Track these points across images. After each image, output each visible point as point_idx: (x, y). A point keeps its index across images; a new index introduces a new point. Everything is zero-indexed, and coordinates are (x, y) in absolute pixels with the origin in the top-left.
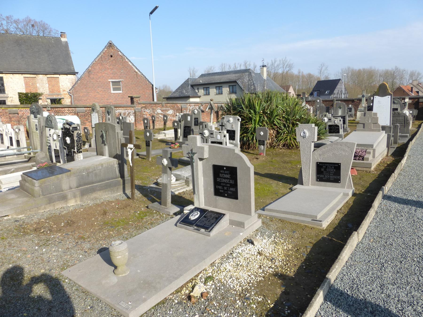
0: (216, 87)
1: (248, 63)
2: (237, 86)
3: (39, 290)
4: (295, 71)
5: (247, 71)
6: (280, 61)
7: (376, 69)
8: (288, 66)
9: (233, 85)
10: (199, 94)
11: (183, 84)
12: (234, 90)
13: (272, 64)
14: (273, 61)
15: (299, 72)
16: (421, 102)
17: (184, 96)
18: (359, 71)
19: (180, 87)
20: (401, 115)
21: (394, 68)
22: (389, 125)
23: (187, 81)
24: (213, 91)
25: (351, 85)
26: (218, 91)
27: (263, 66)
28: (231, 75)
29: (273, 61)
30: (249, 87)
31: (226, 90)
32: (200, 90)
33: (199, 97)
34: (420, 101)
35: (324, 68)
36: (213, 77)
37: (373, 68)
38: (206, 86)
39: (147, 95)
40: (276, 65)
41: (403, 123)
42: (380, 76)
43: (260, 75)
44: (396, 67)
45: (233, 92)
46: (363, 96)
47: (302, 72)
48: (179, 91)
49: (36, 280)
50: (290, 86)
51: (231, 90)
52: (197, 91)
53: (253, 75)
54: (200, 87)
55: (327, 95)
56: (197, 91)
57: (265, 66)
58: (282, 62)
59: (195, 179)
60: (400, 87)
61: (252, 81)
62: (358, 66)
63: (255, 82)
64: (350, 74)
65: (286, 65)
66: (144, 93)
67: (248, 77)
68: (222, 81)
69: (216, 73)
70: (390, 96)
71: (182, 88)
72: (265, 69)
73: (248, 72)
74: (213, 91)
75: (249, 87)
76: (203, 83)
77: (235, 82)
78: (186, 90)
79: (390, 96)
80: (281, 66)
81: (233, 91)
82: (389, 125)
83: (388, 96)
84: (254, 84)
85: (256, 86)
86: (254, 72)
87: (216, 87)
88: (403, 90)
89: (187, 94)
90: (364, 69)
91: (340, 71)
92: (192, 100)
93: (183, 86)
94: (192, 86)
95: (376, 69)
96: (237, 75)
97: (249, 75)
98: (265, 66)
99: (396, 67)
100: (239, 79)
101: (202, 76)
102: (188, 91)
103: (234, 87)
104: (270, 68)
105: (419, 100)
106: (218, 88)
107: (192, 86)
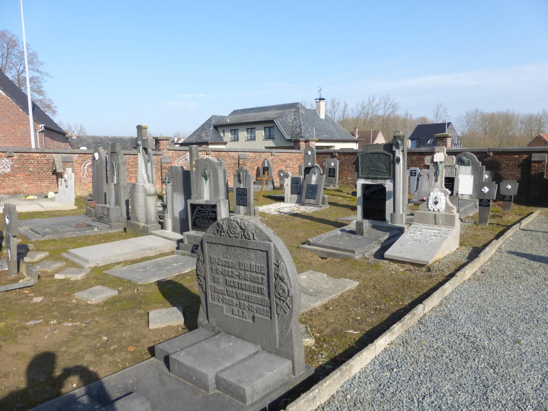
0: (247, 129)
1: (336, 101)
3: (73, 386)
4: (401, 113)
5: (294, 106)
6: (380, 99)
8: (391, 106)
9: (269, 125)
10: (225, 139)
11: (204, 125)
12: (272, 134)
13: (370, 103)
14: (371, 100)
15: (407, 115)
16: (535, 162)
17: (202, 141)
19: (199, 128)
21: (541, 112)
23: (210, 120)
24: (243, 135)
25: (480, 133)
26: (249, 135)
27: (320, 99)
28: (271, 112)
29: (371, 100)
30: (292, 130)
31: (260, 133)
32: (225, 133)
33: (225, 144)
34: (533, 159)
35: (441, 110)
36: (248, 114)
37: (511, 112)
38: (234, 127)
39: (19, 135)
40: (374, 104)
41: (265, 288)
42: (522, 123)
43: (314, 113)
44: (544, 110)
45: (269, 137)
47: (411, 115)
48: (197, 134)
49: (68, 372)
50: (378, 132)
51: (268, 134)
52: (222, 135)
53: (302, 111)
54: (226, 129)
55: (429, 145)
56: (222, 135)
57: (323, 99)
58: (383, 101)
60: (540, 136)
61: (298, 121)
63: (302, 123)
64: (478, 118)
65: (389, 104)
66: (13, 131)
67: (294, 115)
68: (255, 120)
69: (253, 108)
71: (201, 130)
72: (322, 103)
74: (243, 135)
76: (231, 123)
77: (272, 121)
78: (205, 133)
80: (382, 105)
81: (270, 136)
84: (301, 125)
85: (303, 128)
86: (304, 108)
87: (247, 129)
88: (545, 140)
89: (205, 139)
90: (499, 113)
91: (464, 114)
92: (210, 147)
93: (203, 128)
94: (216, 127)
96: (279, 112)
97: (295, 112)
98: (323, 99)
99: (544, 110)
100: (279, 117)
101: (235, 112)
102: (209, 135)
103: (271, 129)
104: (367, 108)
105: (530, 157)
106: (250, 130)
107: (216, 127)
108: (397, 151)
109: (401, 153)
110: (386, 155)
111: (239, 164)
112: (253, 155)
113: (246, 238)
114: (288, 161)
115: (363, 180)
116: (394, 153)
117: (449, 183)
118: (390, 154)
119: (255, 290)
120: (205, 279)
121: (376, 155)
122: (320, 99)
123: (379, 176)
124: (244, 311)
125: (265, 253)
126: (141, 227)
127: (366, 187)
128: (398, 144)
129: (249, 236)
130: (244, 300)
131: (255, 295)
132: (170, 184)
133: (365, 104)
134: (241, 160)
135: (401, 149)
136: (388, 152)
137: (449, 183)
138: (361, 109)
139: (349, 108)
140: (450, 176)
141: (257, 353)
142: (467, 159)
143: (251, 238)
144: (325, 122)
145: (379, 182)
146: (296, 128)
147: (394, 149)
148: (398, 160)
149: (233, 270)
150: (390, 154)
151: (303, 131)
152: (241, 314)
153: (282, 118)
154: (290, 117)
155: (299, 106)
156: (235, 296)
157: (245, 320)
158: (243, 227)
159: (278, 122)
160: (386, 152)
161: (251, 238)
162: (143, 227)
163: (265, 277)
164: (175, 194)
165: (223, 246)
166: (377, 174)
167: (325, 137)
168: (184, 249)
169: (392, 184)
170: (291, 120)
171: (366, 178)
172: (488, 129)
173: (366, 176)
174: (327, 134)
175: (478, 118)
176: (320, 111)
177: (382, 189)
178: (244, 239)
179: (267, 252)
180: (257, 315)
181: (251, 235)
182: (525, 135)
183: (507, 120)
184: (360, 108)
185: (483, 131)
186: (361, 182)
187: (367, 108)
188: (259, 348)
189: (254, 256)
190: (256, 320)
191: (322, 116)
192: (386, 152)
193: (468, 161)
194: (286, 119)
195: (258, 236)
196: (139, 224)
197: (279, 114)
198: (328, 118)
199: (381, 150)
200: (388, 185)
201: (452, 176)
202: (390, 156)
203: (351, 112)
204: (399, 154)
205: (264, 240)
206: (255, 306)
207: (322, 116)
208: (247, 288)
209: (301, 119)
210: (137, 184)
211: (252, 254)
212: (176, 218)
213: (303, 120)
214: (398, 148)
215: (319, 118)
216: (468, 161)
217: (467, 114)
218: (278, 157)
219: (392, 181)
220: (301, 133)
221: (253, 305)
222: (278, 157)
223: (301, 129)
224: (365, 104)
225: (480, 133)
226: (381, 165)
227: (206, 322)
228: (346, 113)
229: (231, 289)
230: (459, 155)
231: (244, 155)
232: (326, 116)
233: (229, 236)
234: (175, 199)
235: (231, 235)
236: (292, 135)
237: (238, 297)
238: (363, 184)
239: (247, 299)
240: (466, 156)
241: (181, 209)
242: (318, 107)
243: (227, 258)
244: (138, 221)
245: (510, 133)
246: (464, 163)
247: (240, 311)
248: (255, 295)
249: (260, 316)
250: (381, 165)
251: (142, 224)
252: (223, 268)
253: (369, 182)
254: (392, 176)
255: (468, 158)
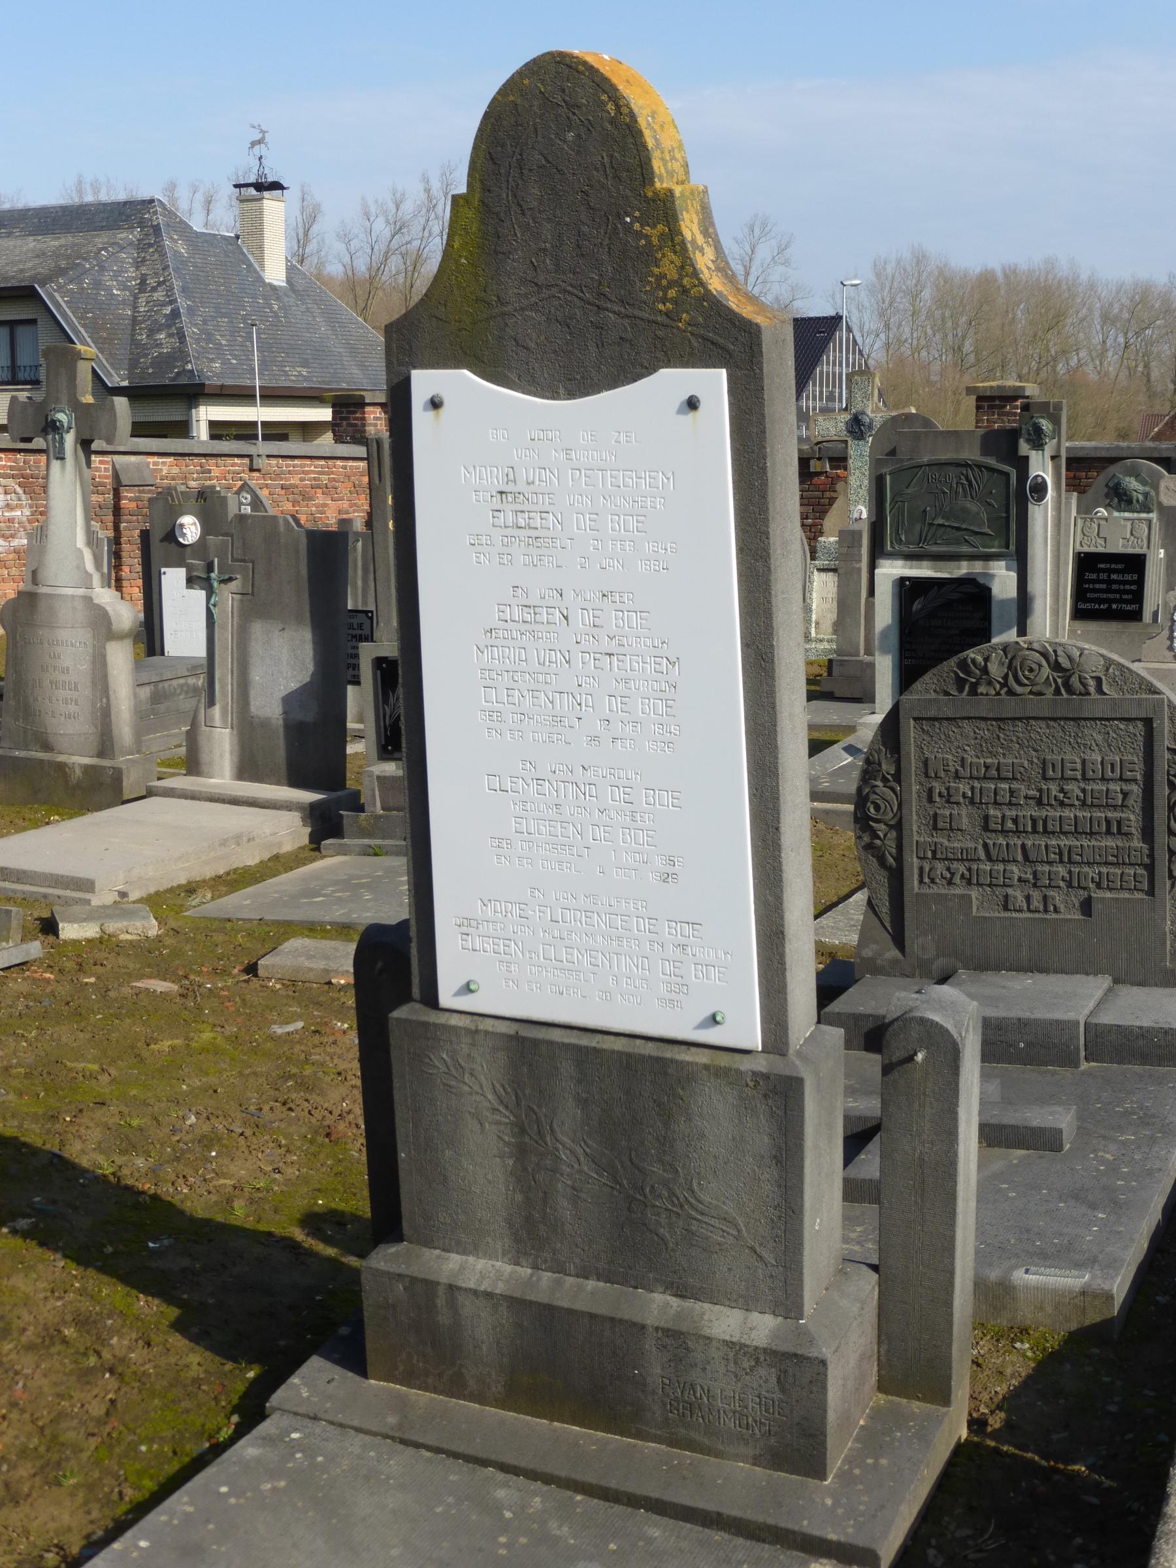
2: (43, 327)
5: (134, 215)
7: (1084, 277)
12: (23, 359)
18: (986, 281)
20: (1094, 706)
22: (746, 1029)
27: (260, 187)
30: (134, 342)
41: (1133, 818)
43: (235, 254)
46: (857, 427)
53: (174, 245)
57: (276, 186)
59: (1062, 562)
61: (159, 295)
62: (974, 252)
63: (183, 303)
64: (927, 294)
67: (138, 264)
70: (713, 384)
72: (273, 208)
73: (142, 224)
75: (134, 342)
77: (26, 294)
79: (713, 384)
81: (14, 367)
82: (746, 1029)
83: (671, 382)
84: (175, 314)
85: (191, 331)
86: (183, 228)
90: (1011, 273)
95: (1084, 277)
96: (52, 243)
97: (142, 246)
98: (276, 186)
100: (61, 272)
103: (21, 331)
104: (416, 228)
108: (1035, 457)
109: (1049, 464)
110: (991, 469)
111: (117, 510)
112: (175, 470)
113: (1070, 691)
114: (320, 498)
115: (900, 563)
116: (1022, 464)
117: (1128, 577)
118: (1006, 468)
119: (1096, 828)
120: (898, 827)
121: (952, 472)
122: (260, 187)
123: (965, 549)
124: (1051, 893)
125: (1140, 724)
126: (78, 772)
127: (907, 589)
128: (1038, 430)
129: (1085, 685)
130: (1050, 863)
131: (1094, 843)
132: (234, 586)
133: (408, 207)
134: (127, 494)
135: (1049, 450)
136: (1001, 460)
137: (1128, 577)
138: (387, 233)
139: (326, 227)
140: (1130, 550)
141: (1110, 990)
142: (1141, 488)
143: (1092, 690)
144: (291, 300)
145: (962, 569)
146: (152, 332)
147: (1024, 448)
148: (1040, 489)
149: (1015, 785)
150: (1006, 468)
151: (192, 347)
152: (1037, 903)
153: (78, 280)
154: (117, 275)
155: (161, 220)
156: (1020, 858)
157: (1054, 916)
158: (1065, 663)
159: (56, 297)
160: (991, 461)
161: (1092, 690)
162: (87, 769)
163: (1136, 790)
164: (257, 629)
165: (983, 724)
166: (958, 542)
167: (296, 376)
168: (364, 833)
169: (1013, 575)
170: (124, 288)
171: (909, 557)
172: (968, 347)
173: (912, 548)
174: (305, 364)
175: (927, 294)
176: (261, 248)
177: (976, 594)
178: (1065, 695)
179: (1148, 722)
180: (1097, 894)
181: (1092, 683)
182: (1123, 375)
183: (1047, 303)
184: (381, 228)
185: (949, 358)
186: (891, 570)
187: (416, 228)
188: (1105, 981)
189: (1099, 738)
190: (1097, 907)
191: (275, 272)
192: (991, 461)
193: (1146, 495)
194: (97, 284)
195: (1114, 682)
196: (61, 758)
197: (56, 255)
198: (300, 283)
199: (972, 453)
200: (1002, 581)
201: (1138, 551)
202: (1007, 475)
203: (340, 247)
204: (1041, 467)
205: (1132, 691)
206: (1091, 872)
207: (275, 272)
208: (1066, 828)
209: (177, 284)
210: (43, 590)
211: (1094, 734)
212: (265, 724)
213: (184, 290)
214: (1037, 442)
215: (260, 279)
216: (1146, 495)
217: (878, 276)
218: (278, 476)
219: (1014, 564)
220: (180, 354)
221: (1086, 869)
222: (278, 476)
223: (181, 337)
224: (408, 207)
225: (936, 367)
226: (972, 506)
227: (894, 953)
228: (312, 247)
229: (1001, 841)
230: (1113, 469)
231: (138, 467)
232: (290, 270)
233: (1011, 693)
234: (257, 648)
235: (1019, 689)
236: (133, 364)
237: (1032, 857)
238: (902, 580)
239: (1065, 857)
240: (1137, 476)
241: (294, 686)
242: (254, 227)
243: (993, 755)
244: (47, 747)
245: (1061, 368)
246: (1130, 502)
247: (1036, 895)
248: (1094, 843)
249: (1108, 895)
250: (972, 506)
251: (80, 760)
252: (977, 784)
253: (923, 571)
254: (1012, 547)
255: (1144, 483)
